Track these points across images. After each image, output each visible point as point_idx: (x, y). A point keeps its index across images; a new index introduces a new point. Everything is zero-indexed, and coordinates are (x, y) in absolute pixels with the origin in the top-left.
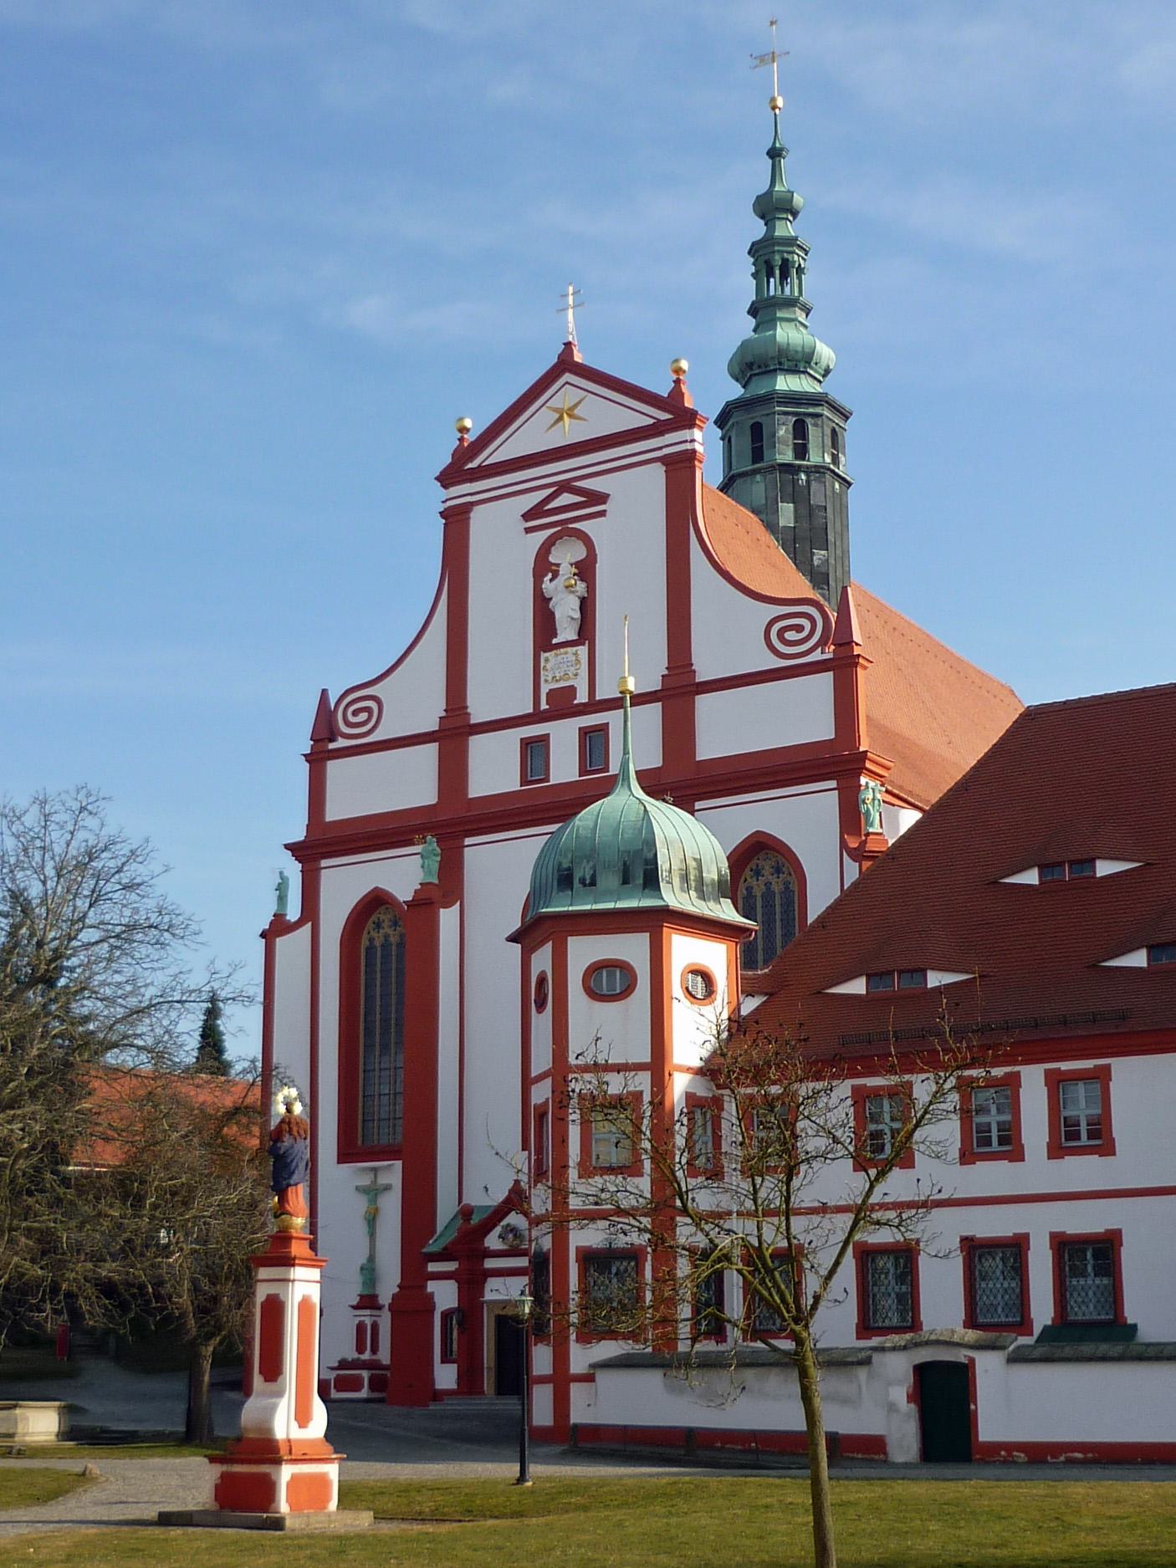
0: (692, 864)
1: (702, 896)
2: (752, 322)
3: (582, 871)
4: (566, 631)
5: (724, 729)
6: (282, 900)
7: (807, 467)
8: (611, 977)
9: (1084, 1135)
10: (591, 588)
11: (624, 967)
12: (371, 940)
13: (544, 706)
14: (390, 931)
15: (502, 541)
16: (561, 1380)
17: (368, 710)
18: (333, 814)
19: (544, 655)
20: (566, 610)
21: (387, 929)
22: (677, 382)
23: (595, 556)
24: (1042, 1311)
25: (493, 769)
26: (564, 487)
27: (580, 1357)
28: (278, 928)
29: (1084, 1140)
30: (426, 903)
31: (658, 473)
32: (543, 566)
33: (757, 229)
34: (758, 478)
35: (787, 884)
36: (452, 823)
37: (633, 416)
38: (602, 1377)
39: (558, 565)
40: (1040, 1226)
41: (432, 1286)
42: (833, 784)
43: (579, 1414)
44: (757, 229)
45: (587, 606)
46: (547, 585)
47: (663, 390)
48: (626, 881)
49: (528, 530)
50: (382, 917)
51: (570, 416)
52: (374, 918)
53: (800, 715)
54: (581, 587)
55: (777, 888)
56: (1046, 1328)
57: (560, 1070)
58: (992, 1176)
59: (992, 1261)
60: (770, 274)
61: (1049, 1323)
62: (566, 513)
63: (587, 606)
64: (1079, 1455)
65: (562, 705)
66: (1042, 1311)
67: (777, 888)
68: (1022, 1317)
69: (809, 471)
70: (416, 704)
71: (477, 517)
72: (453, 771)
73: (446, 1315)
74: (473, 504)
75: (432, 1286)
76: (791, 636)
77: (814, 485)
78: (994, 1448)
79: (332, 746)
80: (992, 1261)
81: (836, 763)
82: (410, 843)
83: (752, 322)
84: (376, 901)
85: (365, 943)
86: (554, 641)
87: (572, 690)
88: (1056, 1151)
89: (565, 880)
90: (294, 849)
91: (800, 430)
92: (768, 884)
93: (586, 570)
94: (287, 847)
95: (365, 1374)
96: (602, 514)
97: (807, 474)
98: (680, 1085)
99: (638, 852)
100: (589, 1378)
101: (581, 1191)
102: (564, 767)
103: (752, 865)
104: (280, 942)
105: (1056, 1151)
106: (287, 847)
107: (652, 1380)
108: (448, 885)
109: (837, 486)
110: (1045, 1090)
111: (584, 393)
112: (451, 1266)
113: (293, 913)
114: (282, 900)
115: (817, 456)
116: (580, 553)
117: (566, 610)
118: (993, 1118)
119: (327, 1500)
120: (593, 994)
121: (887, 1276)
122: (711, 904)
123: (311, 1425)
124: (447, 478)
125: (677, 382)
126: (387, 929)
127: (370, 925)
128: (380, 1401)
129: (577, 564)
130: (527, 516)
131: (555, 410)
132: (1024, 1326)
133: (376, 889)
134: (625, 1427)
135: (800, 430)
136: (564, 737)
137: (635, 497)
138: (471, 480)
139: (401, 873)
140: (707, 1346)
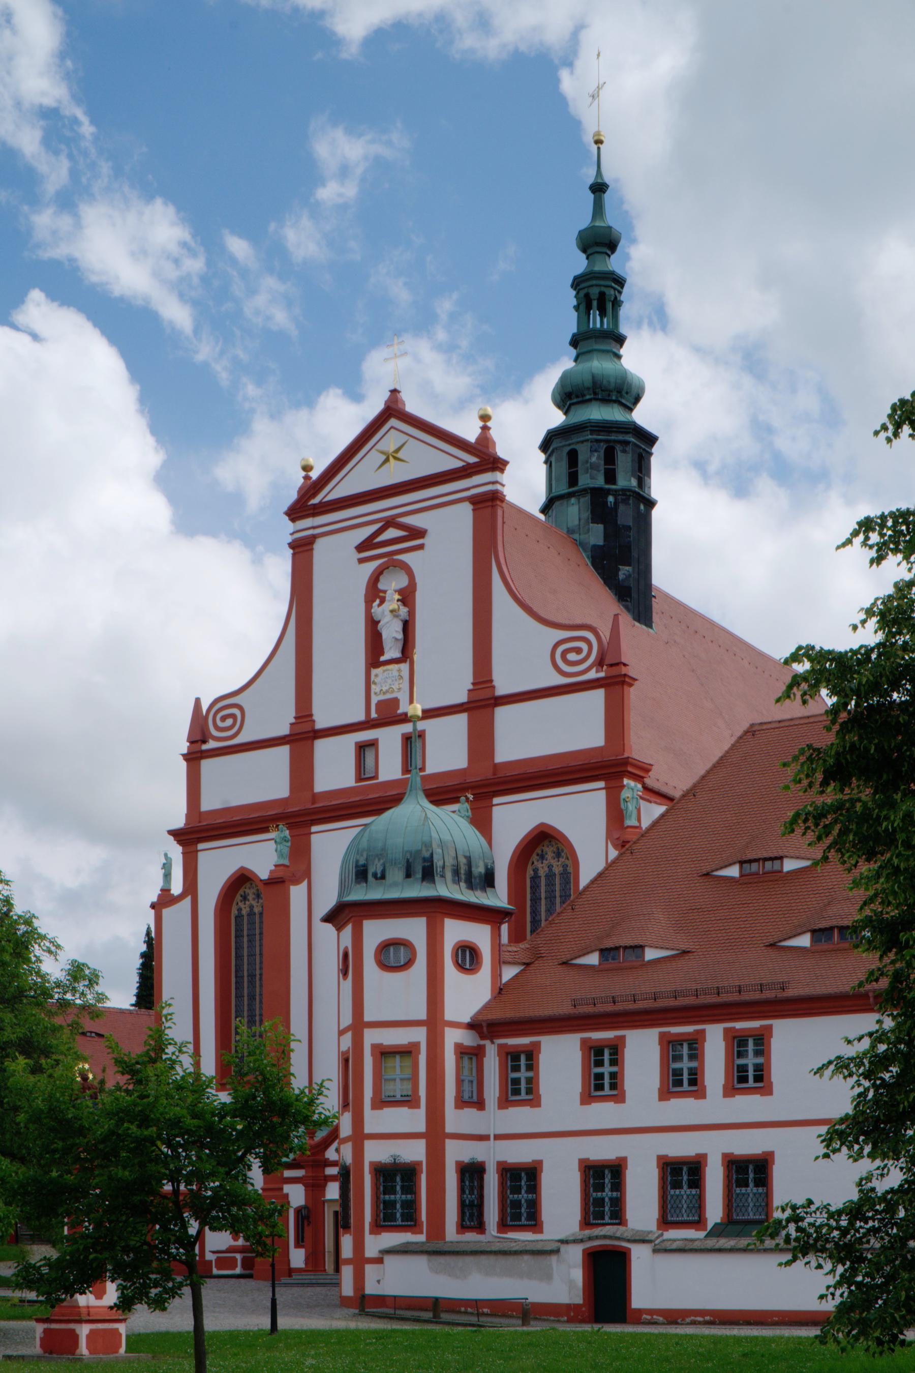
0: (463, 861)
1: (471, 886)
2: (573, 352)
3: (375, 867)
4: (391, 651)
5: (522, 737)
6: (167, 876)
7: (616, 491)
8: (396, 953)
9: (751, 1079)
10: (412, 613)
11: (405, 944)
12: (240, 910)
13: (374, 715)
14: (254, 903)
15: (340, 566)
16: (360, 1261)
17: (233, 716)
18: (208, 803)
19: (374, 672)
20: (391, 631)
21: (251, 900)
22: (485, 429)
23: (415, 584)
24: (714, 1212)
25: (334, 768)
26: (390, 523)
27: (374, 1244)
28: (165, 900)
29: (751, 1083)
30: (279, 882)
31: (465, 512)
32: (374, 593)
33: (579, 263)
34: (573, 500)
35: (565, 866)
36: (300, 815)
37: (445, 460)
38: (388, 1259)
39: (385, 592)
40: (714, 1149)
41: (287, 1188)
42: (602, 784)
43: (371, 1288)
44: (579, 263)
45: (408, 627)
46: (376, 610)
47: (470, 432)
48: (408, 875)
49: (361, 561)
50: (247, 891)
51: (395, 458)
52: (241, 892)
53: (577, 725)
54: (404, 611)
55: (557, 870)
56: (716, 1224)
57: (358, 1025)
58: (683, 1109)
59: (681, 1175)
60: (589, 308)
61: (719, 1221)
62: (390, 547)
63: (408, 627)
64: (700, 1319)
65: (388, 715)
66: (714, 1212)
67: (557, 870)
68: (700, 1217)
69: (615, 493)
70: (273, 716)
71: (320, 546)
72: (302, 770)
73: (298, 1211)
74: (314, 538)
75: (287, 1188)
76: (572, 657)
77: (622, 508)
78: (640, 1311)
79: (205, 747)
80: (681, 1175)
81: (607, 768)
82: (265, 830)
83: (573, 352)
84: (241, 880)
85: (234, 912)
86: (382, 659)
87: (395, 702)
88: (730, 1091)
89: (362, 874)
90: (177, 834)
91: (610, 458)
92: (550, 867)
93: (407, 597)
94: (171, 832)
95: (239, 1257)
96: (421, 547)
97: (615, 496)
98: (453, 1038)
99: (419, 852)
100: (379, 1261)
101: (374, 1120)
102: (390, 768)
103: (538, 851)
104: (166, 912)
105: (730, 1091)
106: (171, 832)
107: (421, 1262)
108: (298, 865)
109: (642, 507)
110: (723, 1043)
111: (406, 437)
112: (300, 1173)
113: (177, 888)
114: (167, 876)
115: (626, 480)
116: (402, 581)
117: (391, 631)
118: (685, 1065)
119: (120, 1346)
120: (385, 966)
121: (603, 1183)
122: (478, 893)
123: (105, 1297)
124: (296, 512)
125: (485, 429)
126: (251, 900)
127: (238, 898)
128: (250, 1276)
129: (400, 592)
130: (361, 548)
131: (382, 453)
132: (699, 1223)
133: (242, 868)
134: (449, 1299)
135: (610, 458)
136: (390, 739)
137: (449, 531)
138: (314, 515)
139: (261, 855)
140: (471, 1237)
